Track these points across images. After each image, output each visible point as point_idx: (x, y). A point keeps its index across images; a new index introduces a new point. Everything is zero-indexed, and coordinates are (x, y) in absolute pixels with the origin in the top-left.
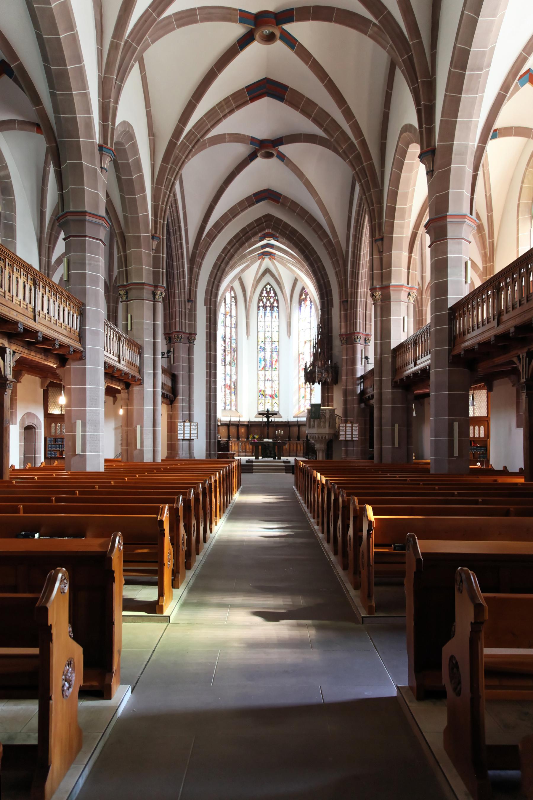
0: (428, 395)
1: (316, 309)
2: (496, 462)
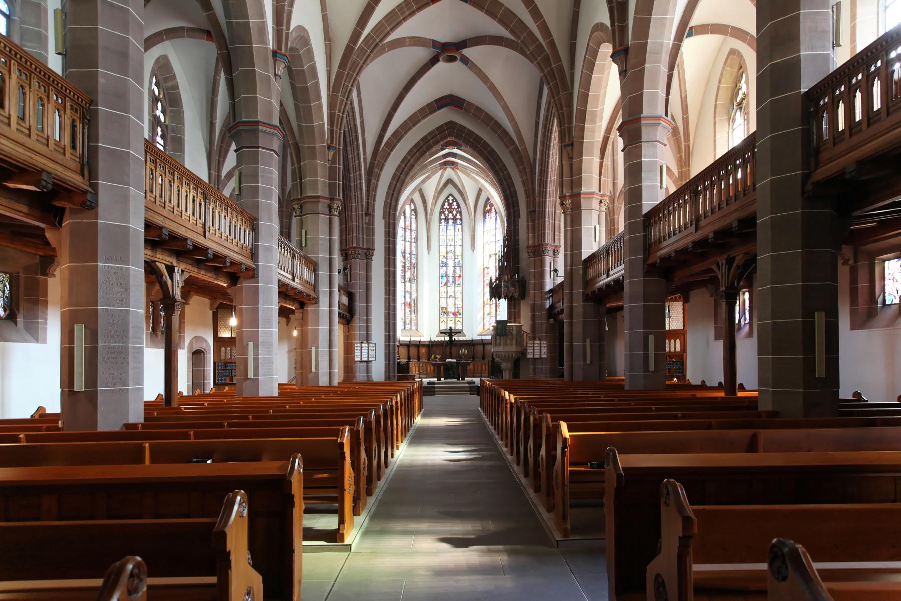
0: (621, 308)
1: (502, 221)
2: (693, 376)
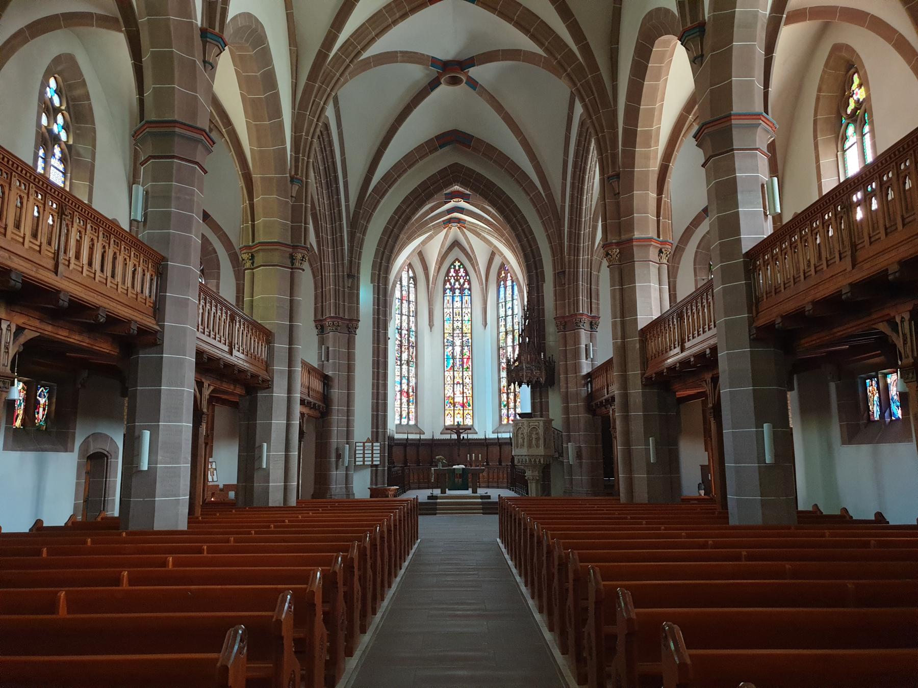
1: (521, 291)
